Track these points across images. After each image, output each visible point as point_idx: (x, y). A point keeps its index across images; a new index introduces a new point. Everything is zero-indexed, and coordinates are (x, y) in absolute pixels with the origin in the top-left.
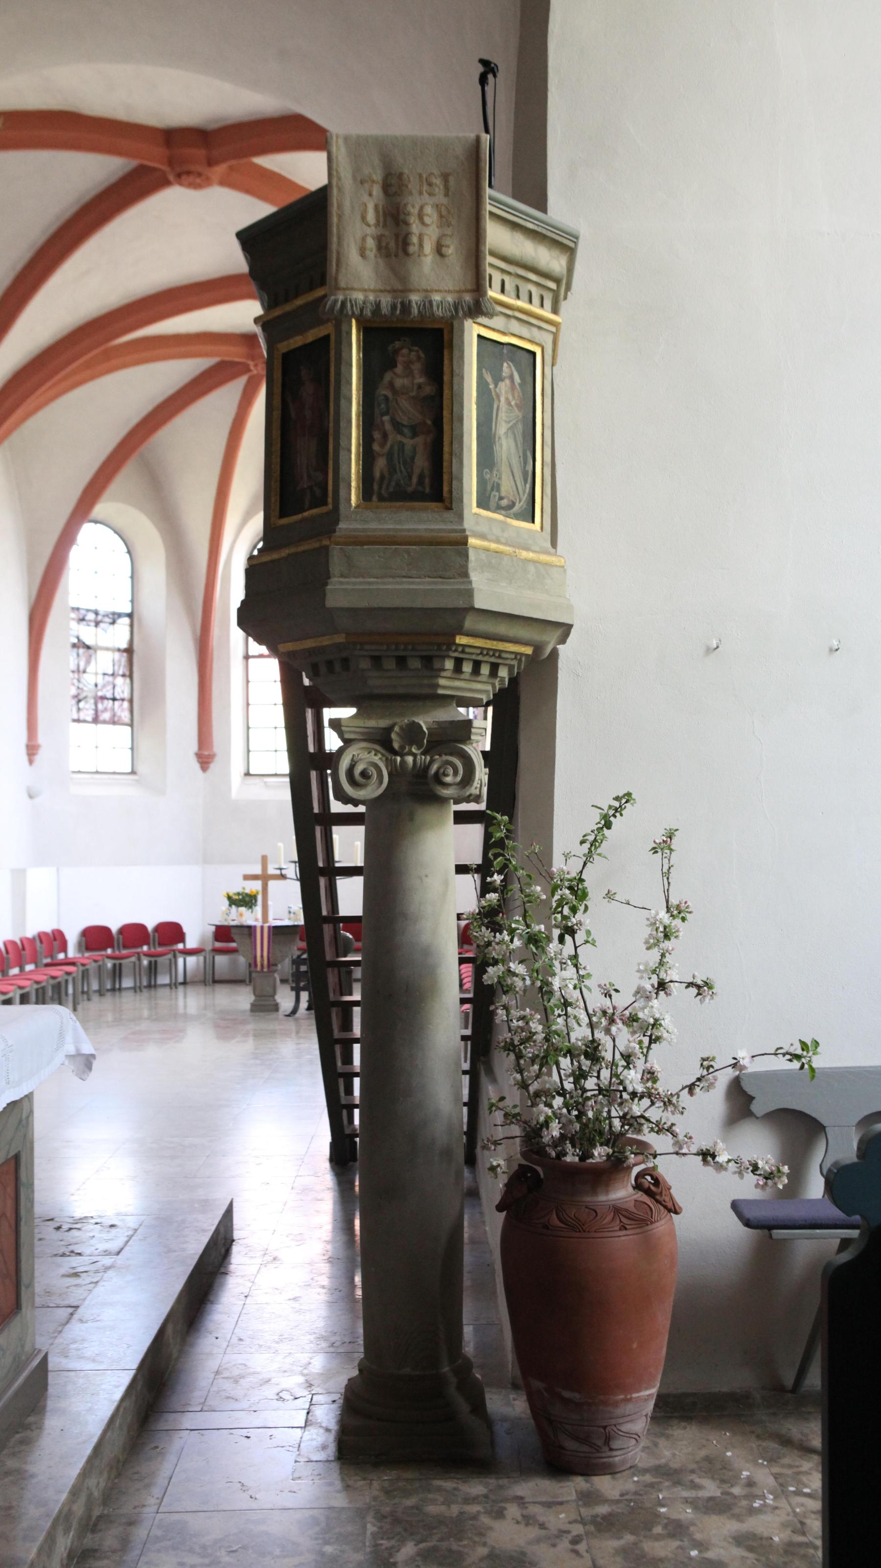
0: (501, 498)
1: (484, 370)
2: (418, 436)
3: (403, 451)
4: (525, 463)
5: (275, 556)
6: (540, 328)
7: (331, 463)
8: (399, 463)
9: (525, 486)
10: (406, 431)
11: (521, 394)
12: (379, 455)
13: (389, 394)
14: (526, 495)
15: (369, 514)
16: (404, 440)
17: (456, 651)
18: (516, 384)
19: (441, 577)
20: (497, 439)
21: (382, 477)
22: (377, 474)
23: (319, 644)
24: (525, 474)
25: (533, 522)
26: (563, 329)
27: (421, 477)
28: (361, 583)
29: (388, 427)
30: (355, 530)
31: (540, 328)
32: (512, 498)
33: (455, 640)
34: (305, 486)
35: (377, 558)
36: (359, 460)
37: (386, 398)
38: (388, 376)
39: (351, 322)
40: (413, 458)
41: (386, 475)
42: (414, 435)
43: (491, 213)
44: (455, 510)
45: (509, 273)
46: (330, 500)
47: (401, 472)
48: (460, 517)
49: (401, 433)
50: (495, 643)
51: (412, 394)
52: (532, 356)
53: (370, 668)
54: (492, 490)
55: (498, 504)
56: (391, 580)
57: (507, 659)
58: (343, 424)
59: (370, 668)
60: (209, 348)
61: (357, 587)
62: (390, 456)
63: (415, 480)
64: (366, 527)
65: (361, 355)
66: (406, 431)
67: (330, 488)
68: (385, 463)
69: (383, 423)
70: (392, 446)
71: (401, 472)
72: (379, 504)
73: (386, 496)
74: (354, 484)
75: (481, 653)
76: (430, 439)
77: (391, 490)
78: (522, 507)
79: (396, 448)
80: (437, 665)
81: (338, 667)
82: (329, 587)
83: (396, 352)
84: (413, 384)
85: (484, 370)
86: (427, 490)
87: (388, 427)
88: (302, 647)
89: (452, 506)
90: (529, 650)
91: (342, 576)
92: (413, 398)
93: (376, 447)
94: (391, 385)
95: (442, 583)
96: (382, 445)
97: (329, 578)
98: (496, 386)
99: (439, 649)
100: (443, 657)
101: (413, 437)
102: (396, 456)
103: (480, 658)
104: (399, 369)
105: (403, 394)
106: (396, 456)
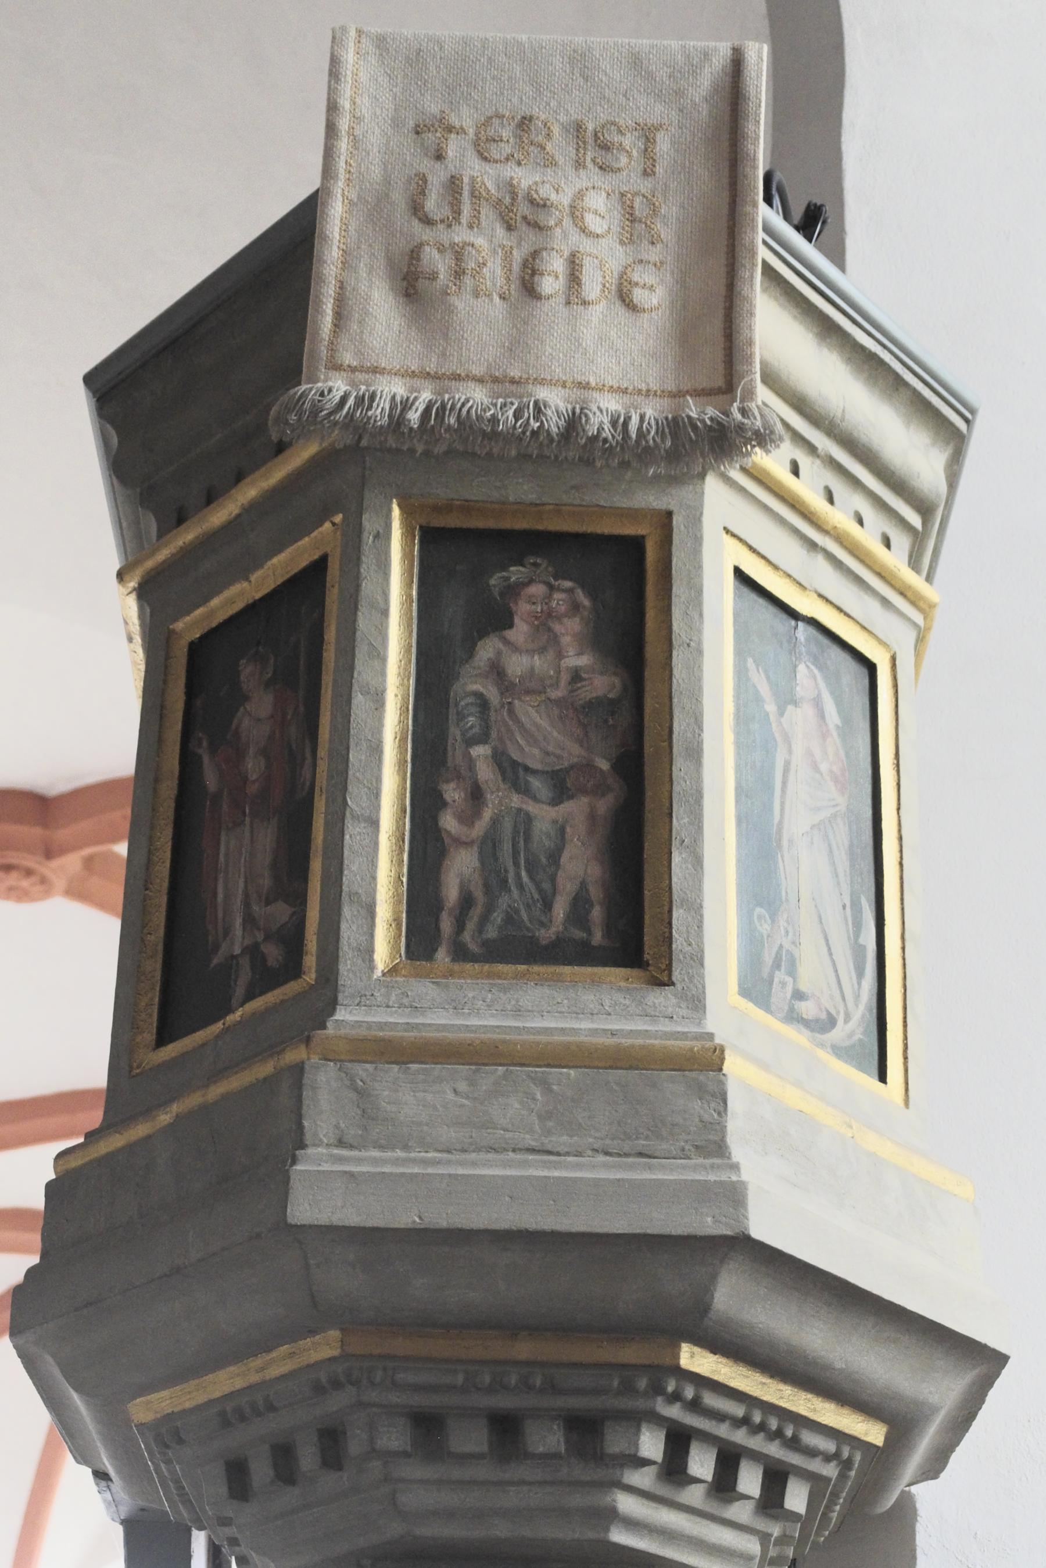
0: (799, 995)
1: (750, 660)
2: (571, 797)
3: (528, 839)
4: (858, 925)
5: (140, 1130)
6: (885, 602)
7: (316, 866)
8: (516, 864)
9: (859, 984)
10: (536, 783)
11: (842, 753)
12: (459, 843)
13: (492, 694)
14: (862, 1007)
15: (425, 990)
16: (531, 807)
17: (676, 1397)
18: (831, 726)
19: (641, 1154)
20: (785, 843)
21: (466, 901)
22: (451, 893)
23: (254, 1378)
24: (858, 951)
25: (883, 1077)
26: (939, 617)
27: (580, 905)
28: (396, 1162)
29: (485, 772)
30: (382, 1026)
31: (885, 602)
32: (828, 1004)
33: (677, 1357)
34: (237, 951)
35: (450, 1096)
36: (401, 850)
37: (483, 704)
38: (487, 650)
39: (390, 511)
40: (555, 857)
41: (479, 894)
42: (561, 791)
43: (768, 269)
44: (679, 986)
45: (811, 449)
46: (310, 961)
47: (521, 886)
48: (697, 1003)
49: (526, 791)
50: (787, 1390)
51: (556, 694)
52: (864, 672)
53: (409, 1448)
54: (777, 965)
55: (792, 1009)
56: (491, 1156)
57: (812, 1453)
58: (356, 757)
59: (409, 1448)
60: (53, 1122)
61: (387, 1169)
62: (489, 846)
63: (560, 910)
64: (419, 1020)
65: (414, 593)
66: (536, 783)
67: (311, 943)
68: (476, 864)
69: (471, 763)
70: (495, 822)
71: (521, 886)
72: (456, 967)
73: (473, 947)
74: (384, 912)
75: (744, 1422)
76: (604, 805)
77: (491, 932)
78: (850, 1035)
79: (507, 826)
80: (615, 1442)
81: (308, 1458)
82: (298, 1167)
83: (513, 591)
84: (558, 672)
85: (750, 660)
86: (598, 937)
87: (485, 772)
88: (201, 1398)
89: (670, 975)
90: (874, 1433)
91: (341, 1143)
92: (557, 702)
93: (449, 822)
94: (497, 671)
95: (650, 1168)
96: (468, 818)
97: (302, 1146)
98: (781, 712)
99: (628, 1388)
100: (636, 1419)
101: (556, 802)
102: (507, 847)
103: (740, 1437)
104: (520, 631)
105: (528, 692)
106: (507, 847)
